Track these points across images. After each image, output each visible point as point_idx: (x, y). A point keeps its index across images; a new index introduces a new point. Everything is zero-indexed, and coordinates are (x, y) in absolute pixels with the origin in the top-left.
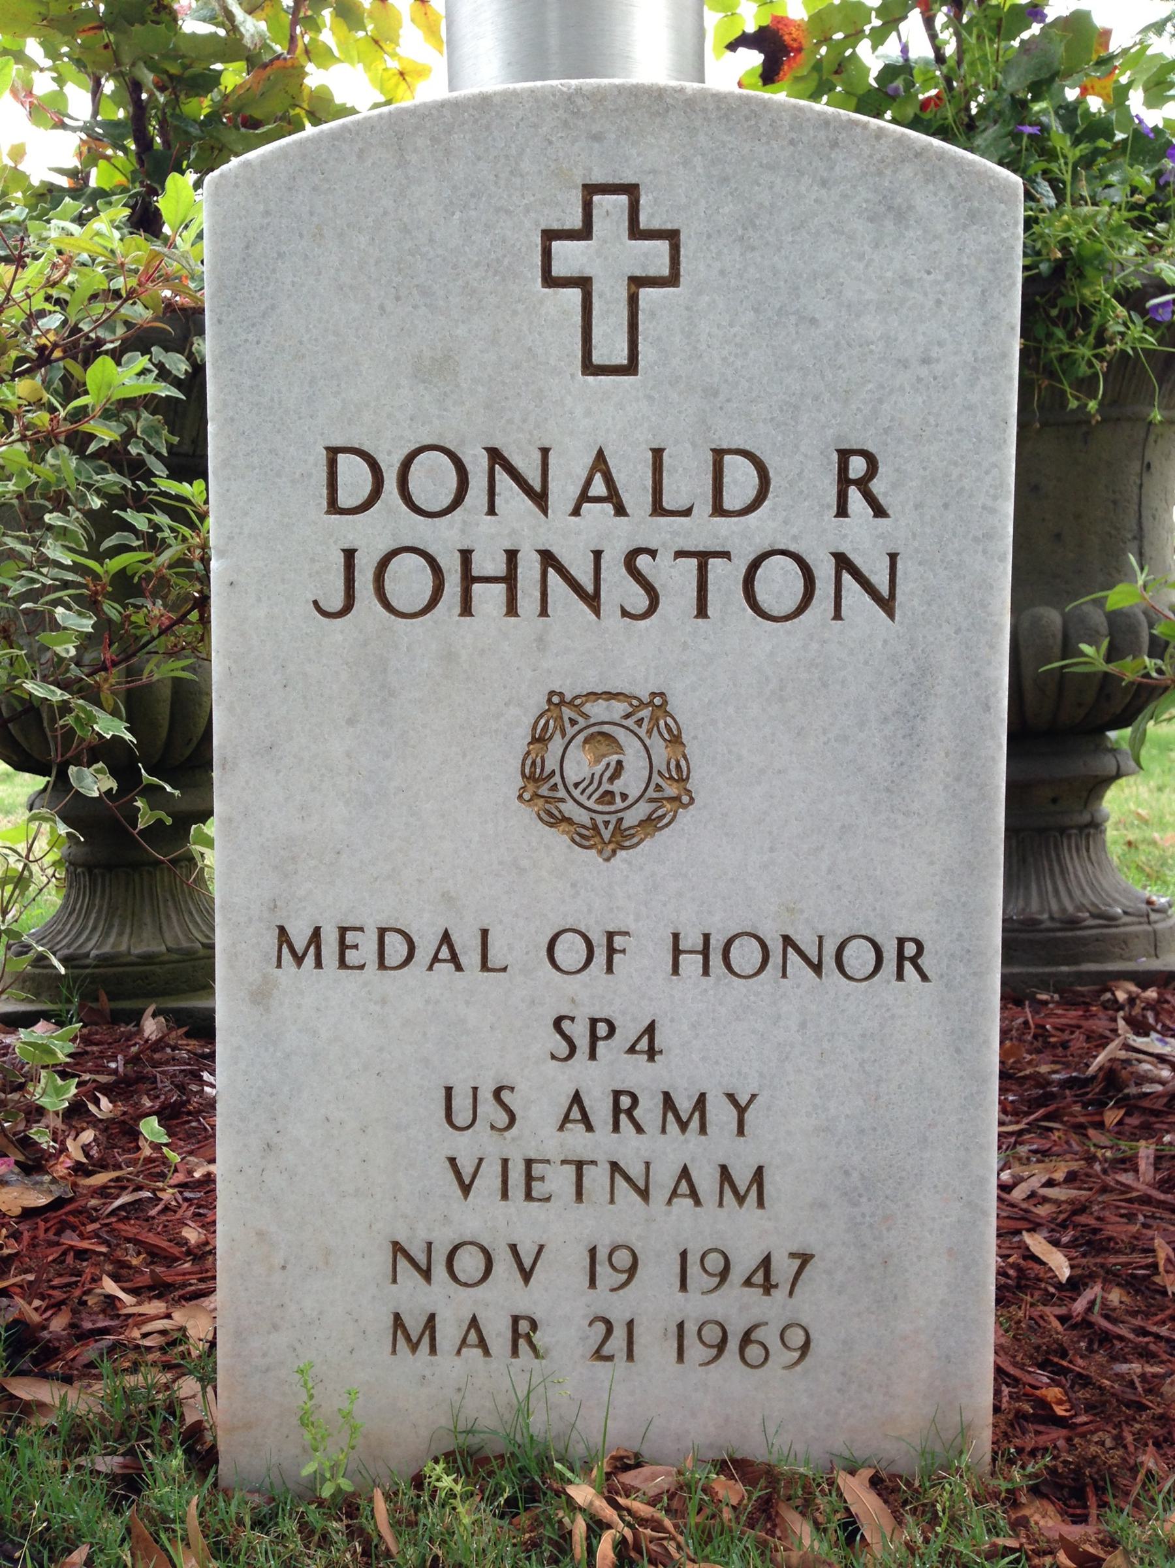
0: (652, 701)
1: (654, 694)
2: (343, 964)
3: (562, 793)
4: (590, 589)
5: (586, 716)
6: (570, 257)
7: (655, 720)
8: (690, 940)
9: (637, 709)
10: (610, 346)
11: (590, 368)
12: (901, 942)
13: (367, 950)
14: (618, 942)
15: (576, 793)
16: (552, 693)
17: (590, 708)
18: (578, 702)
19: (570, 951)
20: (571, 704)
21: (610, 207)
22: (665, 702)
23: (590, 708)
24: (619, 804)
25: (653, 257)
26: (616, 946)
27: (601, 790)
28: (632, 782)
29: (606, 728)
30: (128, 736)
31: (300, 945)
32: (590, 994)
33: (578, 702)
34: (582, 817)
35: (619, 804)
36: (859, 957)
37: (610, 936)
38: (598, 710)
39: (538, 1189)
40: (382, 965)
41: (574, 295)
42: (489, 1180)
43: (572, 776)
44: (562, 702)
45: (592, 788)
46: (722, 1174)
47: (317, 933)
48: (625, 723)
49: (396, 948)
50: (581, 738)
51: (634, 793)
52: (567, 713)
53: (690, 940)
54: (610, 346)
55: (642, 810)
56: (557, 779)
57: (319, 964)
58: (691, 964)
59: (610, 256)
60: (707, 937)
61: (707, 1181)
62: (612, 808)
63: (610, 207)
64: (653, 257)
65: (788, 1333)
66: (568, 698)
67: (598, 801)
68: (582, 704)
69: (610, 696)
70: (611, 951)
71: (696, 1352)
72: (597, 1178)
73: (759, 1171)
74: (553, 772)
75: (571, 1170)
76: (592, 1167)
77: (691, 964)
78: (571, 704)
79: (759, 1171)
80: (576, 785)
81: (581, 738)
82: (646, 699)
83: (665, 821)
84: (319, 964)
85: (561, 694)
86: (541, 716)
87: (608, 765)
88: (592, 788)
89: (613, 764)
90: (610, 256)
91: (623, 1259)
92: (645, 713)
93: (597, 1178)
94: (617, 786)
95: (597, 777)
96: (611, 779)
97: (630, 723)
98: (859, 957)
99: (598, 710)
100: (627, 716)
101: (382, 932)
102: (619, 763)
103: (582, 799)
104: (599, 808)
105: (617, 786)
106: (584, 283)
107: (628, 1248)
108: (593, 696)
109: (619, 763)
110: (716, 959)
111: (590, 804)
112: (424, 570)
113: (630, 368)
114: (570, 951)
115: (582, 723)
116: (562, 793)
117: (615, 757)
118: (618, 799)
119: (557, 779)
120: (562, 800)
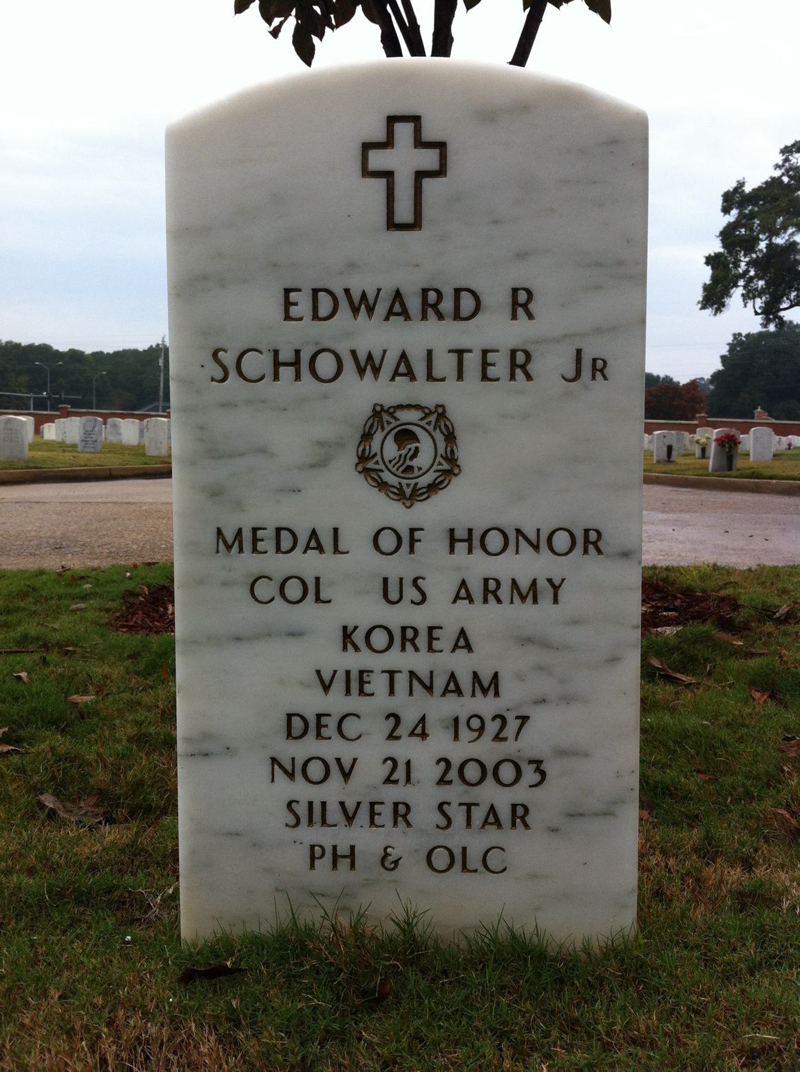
1: (438, 406)
2: (255, 550)
3: (381, 466)
4: (290, 771)
5: (396, 419)
6: (378, 160)
9: (427, 415)
10: (404, 212)
11: (392, 225)
14: (417, 535)
15: (390, 466)
17: (399, 414)
19: (387, 541)
20: (387, 411)
21: (404, 132)
22: (444, 411)
23: (399, 414)
24: (416, 473)
28: (424, 458)
30: (294, 13)
31: (230, 539)
32: (399, 567)
33: (392, 410)
35: (416, 473)
36: (562, 540)
37: (412, 531)
39: (367, 688)
42: (339, 684)
43: (387, 456)
44: (382, 409)
46: (474, 678)
47: (240, 531)
48: (420, 423)
49: (286, 542)
51: (425, 466)
52: (386, 417)
54: (404, 212)
61: (465, 682)
63: (404, 132)
64: (429, 159)
66: (385, 409)
67: (403, 472)
69: (409, 406)
70: (413, 541)
71: (464, 733)
72: (401, 681)
73: (496, 675)
74: (376, 454)
75: (386, 676)
76: (400, 674)
78: (387, 411)
79: (496, 675)
80: (390, 461)
82: (433, 410)
84: (241, 550)
85: (381, 405)
86: (358, 447)
87: (410, 449)
92: (433, 418)
93: (401, 681)
95: (403, 456)
97: (423, 423)
98: (562, 540)
102: (417, 448)
103: (394, 470)
104: (403, 475)
106: (388, 175)
108: (401, 407)
109: (417, 448)
110: (476, 542)
111: (399, 473)
112: (285, 369)
113: (416, 225)
114: (387, 541)
115: (394, 423)
116: (381, 466)
117: (413, 446)
118: (416, 469)
119: (378, 458)
120: (382, 471)
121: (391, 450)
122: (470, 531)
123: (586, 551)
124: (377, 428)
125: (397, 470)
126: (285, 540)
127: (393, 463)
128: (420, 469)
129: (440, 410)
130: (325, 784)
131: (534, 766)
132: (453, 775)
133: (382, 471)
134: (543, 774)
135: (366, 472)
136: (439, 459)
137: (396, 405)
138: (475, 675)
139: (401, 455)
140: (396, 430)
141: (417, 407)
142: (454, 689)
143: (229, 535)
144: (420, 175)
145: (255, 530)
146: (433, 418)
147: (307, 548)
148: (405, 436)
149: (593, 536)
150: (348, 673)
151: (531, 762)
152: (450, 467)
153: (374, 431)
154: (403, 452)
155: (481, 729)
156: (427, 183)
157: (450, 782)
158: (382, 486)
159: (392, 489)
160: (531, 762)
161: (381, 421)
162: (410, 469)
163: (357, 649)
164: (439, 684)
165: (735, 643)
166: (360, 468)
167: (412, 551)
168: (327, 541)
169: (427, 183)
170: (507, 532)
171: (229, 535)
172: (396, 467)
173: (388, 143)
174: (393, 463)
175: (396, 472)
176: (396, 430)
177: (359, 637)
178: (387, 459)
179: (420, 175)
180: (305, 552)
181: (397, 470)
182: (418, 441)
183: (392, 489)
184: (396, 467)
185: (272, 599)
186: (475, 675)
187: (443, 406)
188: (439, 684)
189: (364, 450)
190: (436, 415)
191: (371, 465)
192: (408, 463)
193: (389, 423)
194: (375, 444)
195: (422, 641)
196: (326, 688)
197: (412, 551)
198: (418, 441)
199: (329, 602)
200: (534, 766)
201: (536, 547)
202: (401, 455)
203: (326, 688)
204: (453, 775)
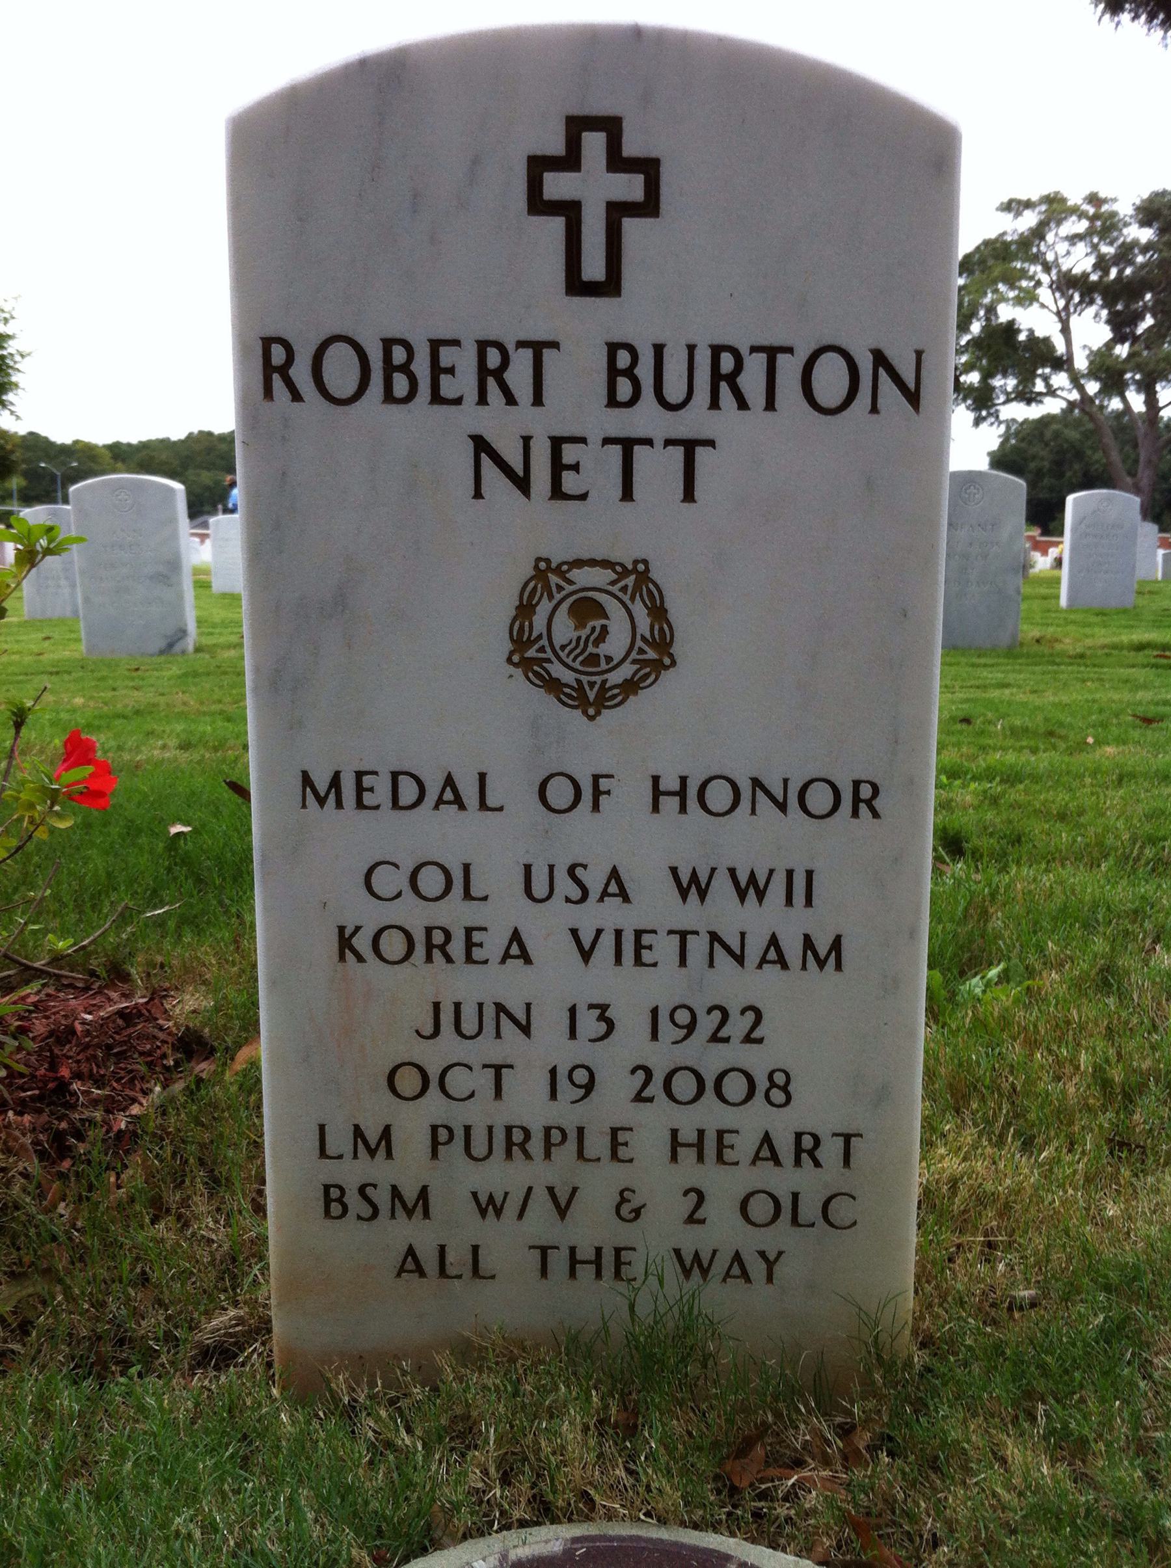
0: (635, 568)
1: (636, 562)
2: (360, 805)
3: (549, 654)
5: (570, 582)
6: (557, 185)
7: (637, 587)
8: (670, 783)
10: (594, 268)
11: (577, 285)
12: (857, 784)
13: (381, 793)
16: (539, 560)
17: (575, 574)
18: (565, 567)
21: (594, 144)
25: (631, 187)
26: (445, 362)
27: (586, 654)
28: (616, 644)
29: (590, 594)
31: (322, 789)
33: (565, 567)
34: (568, 677)
36: (820, 798)
38: (584, 577)
40: (395, 804)
41: (557, 225)
43: (558, 640)
45: (578, 651)
48: (610, 588)
49: (408, 792)
50: (565, 606)
52: (554, 579)
53: (670, 783)
54: (594, 268)
55: (626, 671)
56: (544, 642)
57: (339, 804)
58: (670, 804)
59: (594, 185)
60: (683, 780)
61: (793, 949)
62: (599, 669)
63: (594, 144)
64: (631, 187)
65: (833, 1204)
67: (582, 663)
68: (569, 570)
69: (592, 563)
70: (597, 793)
72: (698, 947)
77: (670, 804)
80: (563, 647)
81: (565, 606)
83: (649, 681)
84: (339, 804)
85: (548, 561)
87: (593, 629)
88: (578, 651)
89: (598, 630)
90: (594, 185)
91: (581, 1076)
92: (630, 580)
93: (698, 947)
94: (604, 649)
96: (597, 643)
97: (615, 589)
98: (820, 798)
99: (584, 577)
100: (613, 583)
101: (395, 776)
102: (604, 628)
103: (569, 661)
104: (580, 668)
105: (604, 649)
106: (570, 211)
107: (583, 1066)
108: (579, 563)
111: (577, 665)
113: (611, 286)
117: (598, 623)
120: (549, 661)
121: (564, 630)
122: (683, 780)
123: (855, 813)
124: (542, 595)
125: (574, 660)
126: (407, 791)
127: (568, 649)
128: (609, 659)
129: (641, 567)
130: (672, 1007)
131: (598, 1012)
132: (656, 1088)
133: (549, 661)
134: (611, 1025)
135: (526, 665)
136: (639, 643)
137: (571, 560)
138: (807, 939)
139: (579, 638)
140: (574, 597)
141: (606, 564)
142: (518, 953)
143: (322, 783)
144: (617, 211)
145: (359, 775)
146: (630, 580)
147: (440, 801)
148: (586, 609)
149: (866, 791)
150: (790, 874)
151: (591, 1006)
152: (658, 653)
153: (536, 599)
154: (584, 633)
155: (691, 1028)
156: (631, 226)
157: (650, 1100)
158: (553, 685)
159: (567, 690)
160: (591, 1006)
161: (547, 587)
162: (593, 659)
163: (360, 959)
164: (753, 953)
165: (1001, 966)
166: (516, 658)
167: (596, 807)
168: (470, 793)
169: (631, 226)
170: (737, 782)
171: (322, 783)
172: (572, 656)
173: (617, 162)
174: (568, 649)
175: (571, 663)
176: (574, 597)
177: (362, 943)
178: (557, 644)
179: (617, 211)
180: (436, 807)
181: (574, 660)
182: (607, 618)
183: (567, 690)
184: (572, 656)
185: (399, 895)
186: (807, 939)
187: (645, 562)
188: (753, 953)
189: (521, 628)
190: (633, 577)
191: (531, 653)
192: (591, 649)
193: (560, 588)
194: (539, 622)
195: (457, 948)
196: (586, 955)
197: (596, 807)
198: (607, 618)
199: (485, 898)
200: (598, 1012)
201: (782, 807)
202: (579, 638)
203: (586, 955)
204: (656, 1088)
